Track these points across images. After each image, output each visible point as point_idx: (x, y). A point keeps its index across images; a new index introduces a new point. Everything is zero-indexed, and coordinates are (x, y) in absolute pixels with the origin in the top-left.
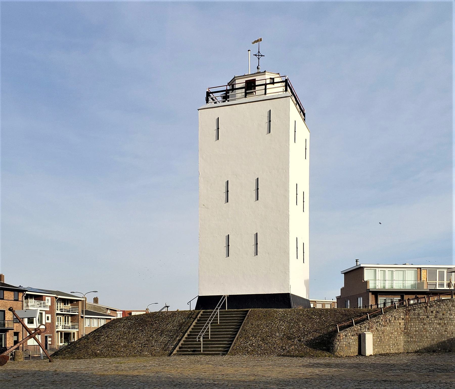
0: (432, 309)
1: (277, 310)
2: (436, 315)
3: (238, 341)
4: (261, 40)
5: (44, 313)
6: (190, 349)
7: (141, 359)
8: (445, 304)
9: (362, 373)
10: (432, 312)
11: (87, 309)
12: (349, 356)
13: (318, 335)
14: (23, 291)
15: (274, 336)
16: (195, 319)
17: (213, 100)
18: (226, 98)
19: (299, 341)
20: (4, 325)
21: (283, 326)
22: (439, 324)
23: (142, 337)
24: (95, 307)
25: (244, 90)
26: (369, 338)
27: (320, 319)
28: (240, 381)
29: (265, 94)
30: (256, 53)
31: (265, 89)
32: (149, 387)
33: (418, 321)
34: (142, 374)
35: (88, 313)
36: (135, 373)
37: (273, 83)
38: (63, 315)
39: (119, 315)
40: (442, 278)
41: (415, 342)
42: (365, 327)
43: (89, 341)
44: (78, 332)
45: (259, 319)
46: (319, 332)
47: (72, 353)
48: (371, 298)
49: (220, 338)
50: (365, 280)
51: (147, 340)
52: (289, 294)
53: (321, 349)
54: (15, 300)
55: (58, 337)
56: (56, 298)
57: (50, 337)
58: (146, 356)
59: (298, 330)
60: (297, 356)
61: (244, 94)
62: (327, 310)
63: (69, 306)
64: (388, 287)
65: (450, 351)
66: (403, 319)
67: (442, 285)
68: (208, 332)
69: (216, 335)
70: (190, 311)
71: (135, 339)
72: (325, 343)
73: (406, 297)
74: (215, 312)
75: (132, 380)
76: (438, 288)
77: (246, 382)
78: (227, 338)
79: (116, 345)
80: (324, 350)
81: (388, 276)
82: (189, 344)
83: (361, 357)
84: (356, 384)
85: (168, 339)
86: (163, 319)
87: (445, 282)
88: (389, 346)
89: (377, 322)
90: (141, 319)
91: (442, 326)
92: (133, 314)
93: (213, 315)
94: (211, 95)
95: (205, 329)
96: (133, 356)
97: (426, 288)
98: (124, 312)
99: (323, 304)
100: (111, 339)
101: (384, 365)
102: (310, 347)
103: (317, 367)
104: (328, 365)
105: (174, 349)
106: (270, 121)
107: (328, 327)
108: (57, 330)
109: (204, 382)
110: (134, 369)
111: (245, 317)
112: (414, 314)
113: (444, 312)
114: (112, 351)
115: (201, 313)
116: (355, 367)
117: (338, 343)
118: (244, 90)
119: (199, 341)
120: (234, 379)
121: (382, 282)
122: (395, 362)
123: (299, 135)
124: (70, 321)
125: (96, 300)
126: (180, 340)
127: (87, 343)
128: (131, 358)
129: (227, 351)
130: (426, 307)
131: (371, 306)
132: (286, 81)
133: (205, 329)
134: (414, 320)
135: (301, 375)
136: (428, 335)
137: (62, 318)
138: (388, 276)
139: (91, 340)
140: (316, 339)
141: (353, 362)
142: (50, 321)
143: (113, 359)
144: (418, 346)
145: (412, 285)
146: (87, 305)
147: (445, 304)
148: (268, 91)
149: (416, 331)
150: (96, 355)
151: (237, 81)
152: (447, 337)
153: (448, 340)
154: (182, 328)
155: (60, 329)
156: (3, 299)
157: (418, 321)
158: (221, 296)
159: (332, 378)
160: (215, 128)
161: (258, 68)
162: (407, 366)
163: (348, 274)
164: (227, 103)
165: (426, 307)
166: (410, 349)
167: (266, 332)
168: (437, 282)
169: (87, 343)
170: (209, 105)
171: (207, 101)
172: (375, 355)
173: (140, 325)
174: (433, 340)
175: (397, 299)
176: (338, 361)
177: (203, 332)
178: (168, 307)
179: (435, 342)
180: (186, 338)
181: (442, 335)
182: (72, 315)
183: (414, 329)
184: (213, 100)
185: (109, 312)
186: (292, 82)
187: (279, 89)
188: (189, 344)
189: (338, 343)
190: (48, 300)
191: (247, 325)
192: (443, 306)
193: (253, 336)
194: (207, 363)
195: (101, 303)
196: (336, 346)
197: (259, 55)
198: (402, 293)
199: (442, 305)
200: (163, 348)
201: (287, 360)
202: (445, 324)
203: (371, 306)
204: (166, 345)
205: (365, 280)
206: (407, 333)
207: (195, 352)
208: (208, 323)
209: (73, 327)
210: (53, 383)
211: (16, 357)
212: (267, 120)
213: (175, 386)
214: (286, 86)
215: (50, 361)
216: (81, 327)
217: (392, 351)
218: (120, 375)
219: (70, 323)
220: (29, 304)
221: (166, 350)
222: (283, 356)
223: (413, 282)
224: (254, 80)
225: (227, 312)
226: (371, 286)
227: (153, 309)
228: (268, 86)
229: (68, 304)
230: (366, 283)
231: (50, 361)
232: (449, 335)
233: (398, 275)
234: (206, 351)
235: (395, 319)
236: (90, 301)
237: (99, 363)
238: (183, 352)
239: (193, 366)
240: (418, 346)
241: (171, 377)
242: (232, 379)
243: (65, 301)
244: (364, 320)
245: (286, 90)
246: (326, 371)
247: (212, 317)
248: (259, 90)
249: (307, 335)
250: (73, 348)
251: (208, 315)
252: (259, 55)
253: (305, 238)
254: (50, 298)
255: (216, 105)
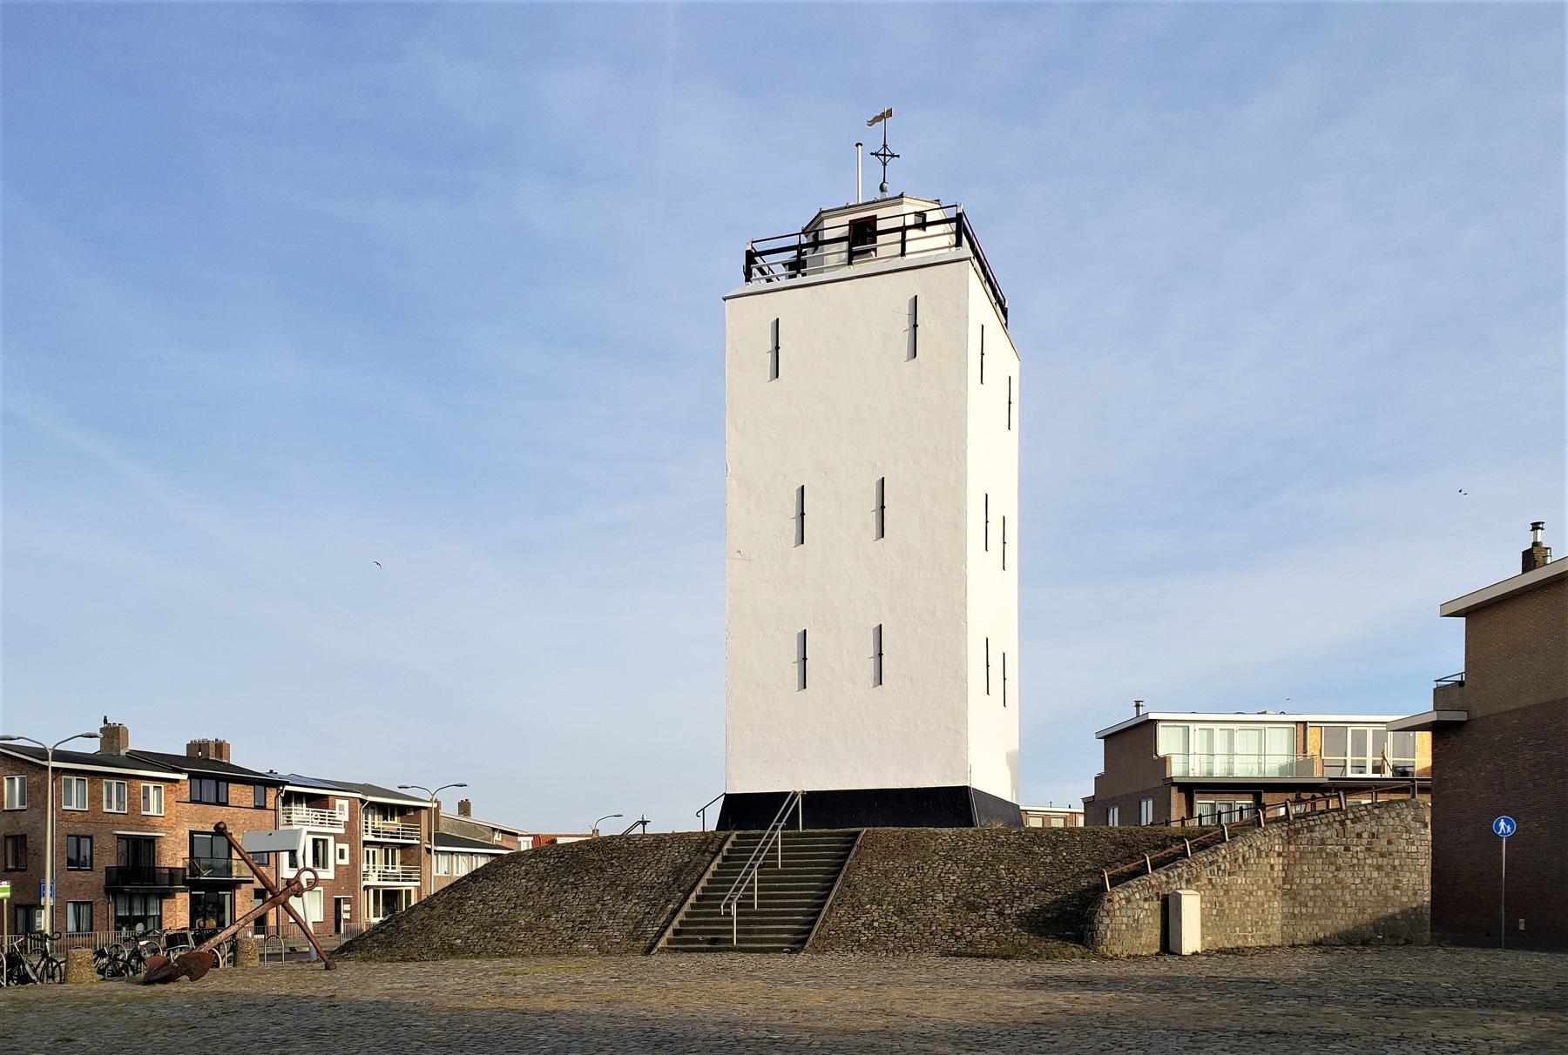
0: (1358, 827)
1: (937, 830)
2: (1370, 843)
3: (833, 915)
4: (889, 113)
5: (331, 840)
6: (704, 937)
7: (572, 962)
8: (1393, 814)
9: (1192, 1006)
10: (1359, 835)
11: (442, 830)
12: (1135, 956)
13: (1050, 898)
14: (276, 784)
15: (929, 900)
16: (716, 854)
17: (763, 273)
18: (796, 266)
19: (1000, 913)
20: (230, 871)
21: (954, 873)
22: (1379, 868)
23: (576, 904)
24: (462, 826)
25: (845, 245)
26: (1191, 906)
27: (1054, 853)
28: (845, 1032)
29: (903, 254)
30: (878, 148)
31: (903, 242)
32: (583, 1050)
33: (1319, 861)
34: (568, 1007)
35: (442, 839)
36: (550, 1004)
37: (922, 225)
38: (381, 844)
39: (525, 844)
40: (1360, 748)
41: (1313, 916)
42: (1180, 876)
43: (435, 912)
44: (419, 889)
45: (889, 854)
46: (1056, 887)
47: (390, 944)
48: (1177, 799)
49: (784, 905)
50: (1161, 753)
51: (588, 912)
52: (966, 788)
53: (1059, 938)
54: (256, 807)
55: (366, 903)
56: (362, 801)
57: (347, 901)
58: (585, 953)
59: (997, 885)
60: (994, 957)
61: (845, 256)
62: (1056, 831)
63: (396, 823)
64: (1219, 771)
65: (1408, 942)
66: (1279, 855)
67: (1361, 767)
68: (752, 889)
69: (772, 897)
70: (703, 833)
71: (557, 908)
72: (1071, 922)
73: (1267, 798)
74: (770, 836)
75: (537, 1027)
76: (1349, 775)
77: (863, 1034)
78: (801, 905)
79: (505, 924)
80: (1066, 939)
81: (1220, 745)
82: (700, 923)
83: (1168, 958)
84: (1184, 1040)
85: (643, 908)
86: (631, 853)
87: (1369, 760)
88: (1244, 928)
89: (1211, 863)
90: (574, 855)
91: (1387, 875)
92: (560, 841)
93: (766, 844)
94: (757, 259)
95: (742, 881)
96: (550, 954)
97: (1318, 775)
98: (536, 838)
99: (1046, 818)
100: (493, 908)
101: (1232, 977)
102: (1031, 932)
103: (1058, 988)
104: (1086, 983)
105: (660, 934)
106: (915, 326)
107: (1076, 876)
108: (366, 883)
109: (741, 1032)
110: (548, 991)
111: (850, 849)
112: (1311, 842)
113: (1393, 836)
114: (495, 940)
115: (733, 838)
116: (1164, 988)
117: (1107, 921)
118: (845, 245)
119: (729, 914)
120: (828, 1024)
121: (1204, 759)
122: (1273, 975)
123: (992, 368)
124: (398, 860)
125: (464, 807)
126: (675, 912)
127: (430, 917)
128: (546, 960)
129: (804, 941)
130: (1342, 823)
131: (1200, 817)
132: (958, 219)
133: (742, 881)
134: (1310, 856)
135: (1017, 1013)
136: (1348, 898)
137: (380, 853)
138: (1220, 745)
139: (440, 909)
140: (1044, 909)
141: (1154, 973)
142: (346, 861)
143: (497, 961)
144: (1322, 929)
145: (1282, 768)
146: (442, 821)
147: (1393, 814)
148: (909, 247)
149: (1315, 887)
150: (453, 952)
151: (827, 223)
152: (1401, 903)
153: (1404, 912)
154: (681, 877)
155: (373, 880)
156: (226, 804)
157: (1319, 861)
158: (777, 798)
159: (1108, 1021)
160: (770, 346)
161: (882, 189)
162: (1311, 986)
163: (1113, 739)
164: (800, 280)
165: (1342, 823)
166: (1300, 935)
167: (908, 890)
168: (1349, 758)
169: (430, 917)
170: (752, 287)
171: (748, 275)
172: (1207, 953)
173: (569, 870)
174: (1362, 911)
175: (1246, 801)
176: (1110, 970)
177: (737, 889)
178: (644, 823)
179: (1367, 917)
180: (692, 906)
181: (1386, 898)
182: (403, 846)
183: (1311, 881)
184: (763, 273)
185: (497, 837)
186: (973, 222)
187: (938, 240)
188: (700, 923)
189: (1107, 921)
190: (342, 807)
191: (861, 871)
192: (1389, 820)
193: (872, 901)
194: (749, 976)
195: (478, 816)
196: (1102, 927)
197: (884, 155)
198: (1257, 789)
199: (1386, 815)
200: (631, 934)
201: (967, 968)
202: (1394, 867)
203: (1200, 817)
204: (638, 924)
205: (1161, 753)
206: (1291, 895)
207: (717, 944)
208: (752, 866)
209: (407, 877)
210: (314, 1034)
211: (241, 957)
212: (906, 324)
213: (658, 1045)
214: (958, 227)
215: (327, 968)
216: (425, 877)
217: (1251, 942)
218: (506, 1010)
219: (398, 865)
220: (294, 818)
221: (638, 939)
222: (956, 954)
223: (1284, 760)
224: (873, 220)
225: (801, 835)
226: (1176, 770)
227: (610, 829)
228: (910, 234)
229: (392, 818)
230: (1164, 761)
231: (327, 968)
232: (1404, 899)
233: (1245, 740)
234: (745, 941)
235: (1259, 856)
236: (450, 810)
237: (456, 974)
238: (683, 943)
239: (709, 983)
240: (1322, 929)
241: (649, 1016)
242: (820, 1024)
243: (385, 811)
244: (1173, 858)
245: (959, 244)
246: (1086, 1000)
247: (761, 851)
248: (886, 245)
249: (1020, 898)
250: (403, 929)
251: (749, 844)
252: (884, 155)
253: (1007, 641)
254: (346, 803)
255: (770, 286)
